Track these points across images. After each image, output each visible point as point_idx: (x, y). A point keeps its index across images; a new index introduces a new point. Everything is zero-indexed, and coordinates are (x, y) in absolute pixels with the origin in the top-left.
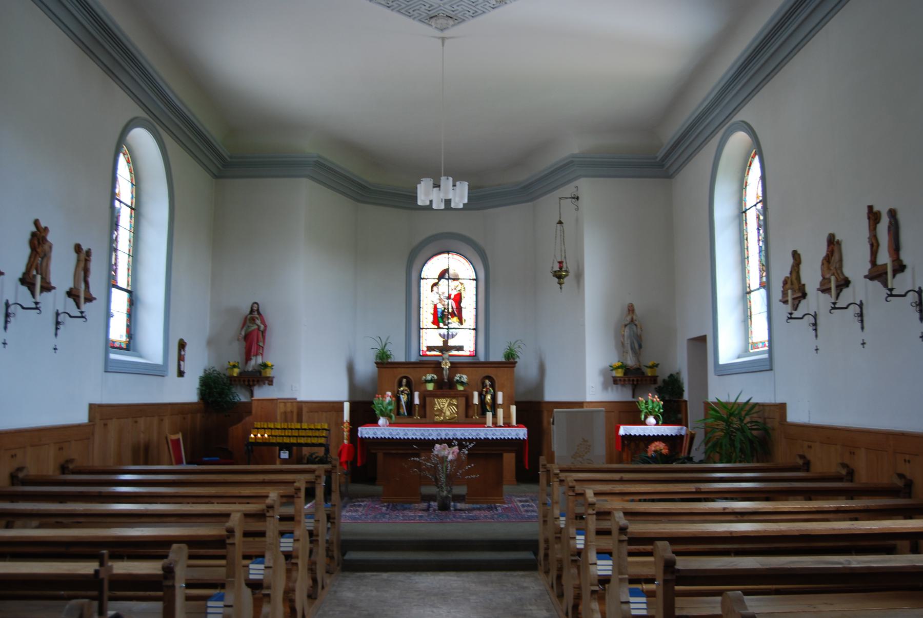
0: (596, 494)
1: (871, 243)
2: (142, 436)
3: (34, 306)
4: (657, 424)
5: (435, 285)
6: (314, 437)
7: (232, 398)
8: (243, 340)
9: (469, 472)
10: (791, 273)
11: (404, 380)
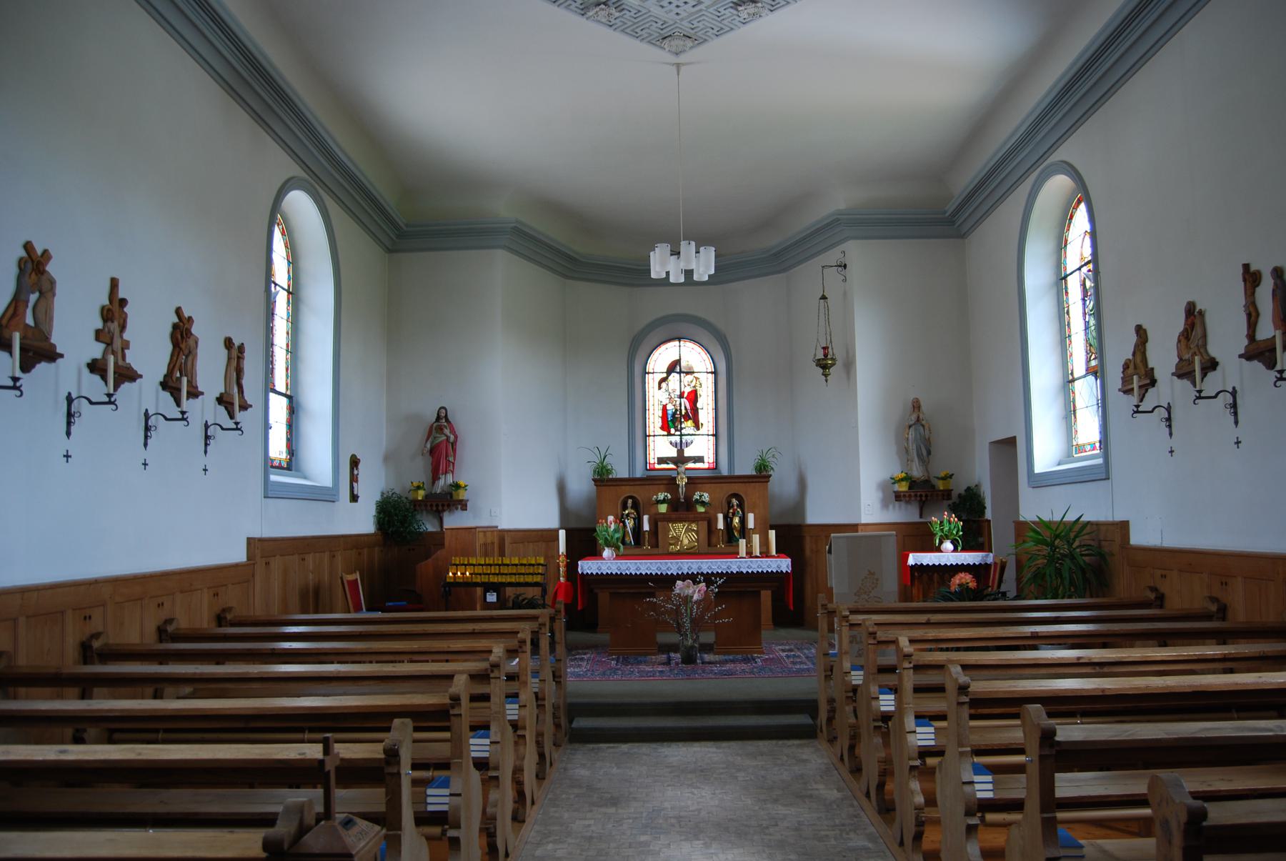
0: (912, 641)
1: (1248, 312)
2: (311, 576)
3: (180, 416)
4: (955, 550)
5: (664, 380)
6: (527, 574)
7: (416, 527)
8: (429, 454)
9: (716, 616)
10: (1134, 354)
11: (630, 501)
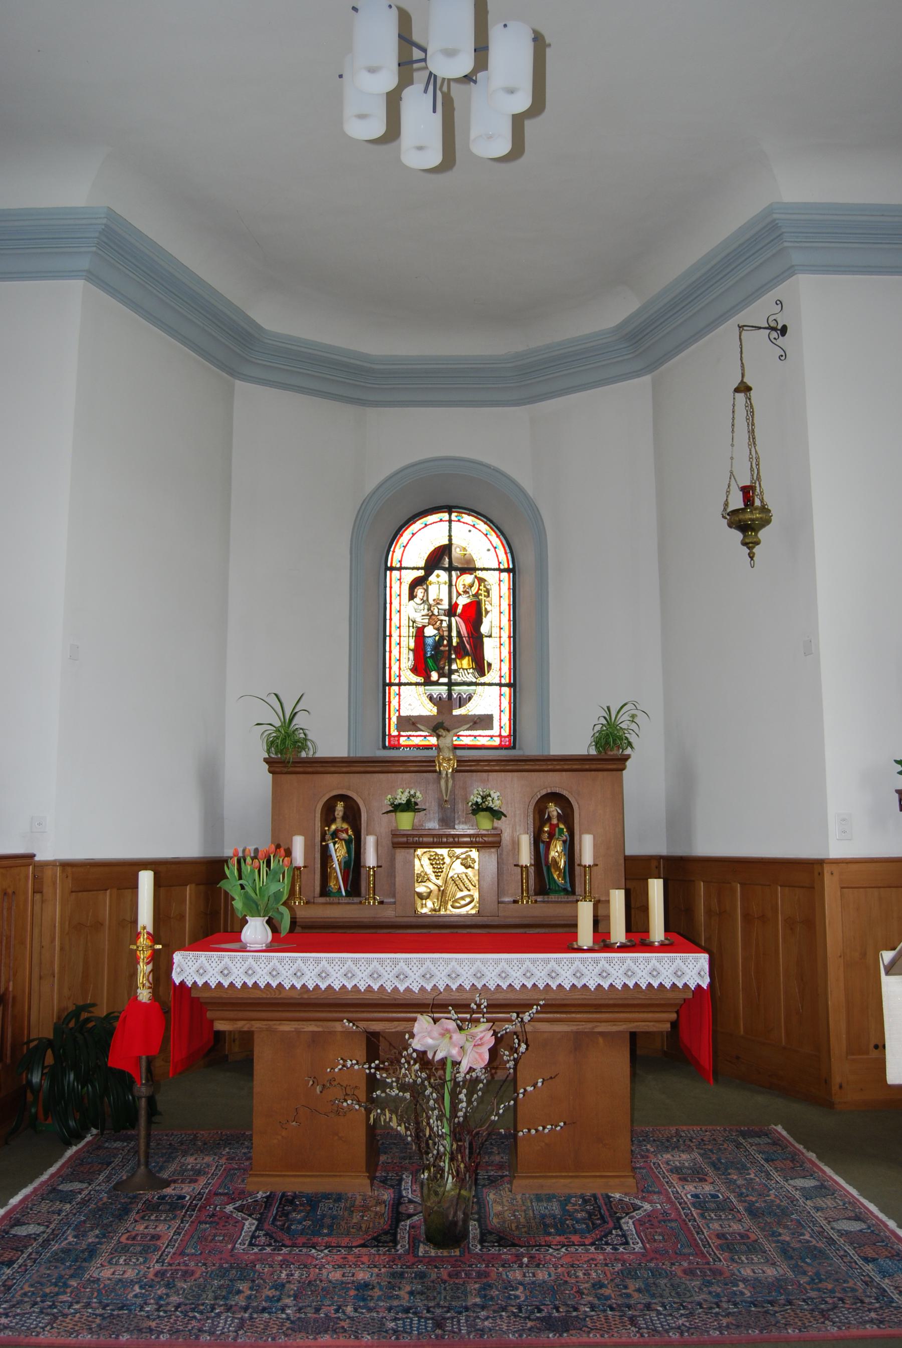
5: (418, 583)
11: (340, 807)
